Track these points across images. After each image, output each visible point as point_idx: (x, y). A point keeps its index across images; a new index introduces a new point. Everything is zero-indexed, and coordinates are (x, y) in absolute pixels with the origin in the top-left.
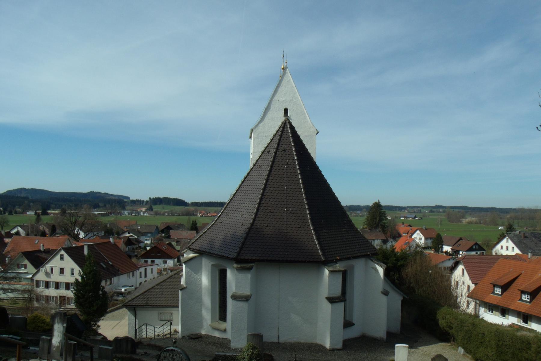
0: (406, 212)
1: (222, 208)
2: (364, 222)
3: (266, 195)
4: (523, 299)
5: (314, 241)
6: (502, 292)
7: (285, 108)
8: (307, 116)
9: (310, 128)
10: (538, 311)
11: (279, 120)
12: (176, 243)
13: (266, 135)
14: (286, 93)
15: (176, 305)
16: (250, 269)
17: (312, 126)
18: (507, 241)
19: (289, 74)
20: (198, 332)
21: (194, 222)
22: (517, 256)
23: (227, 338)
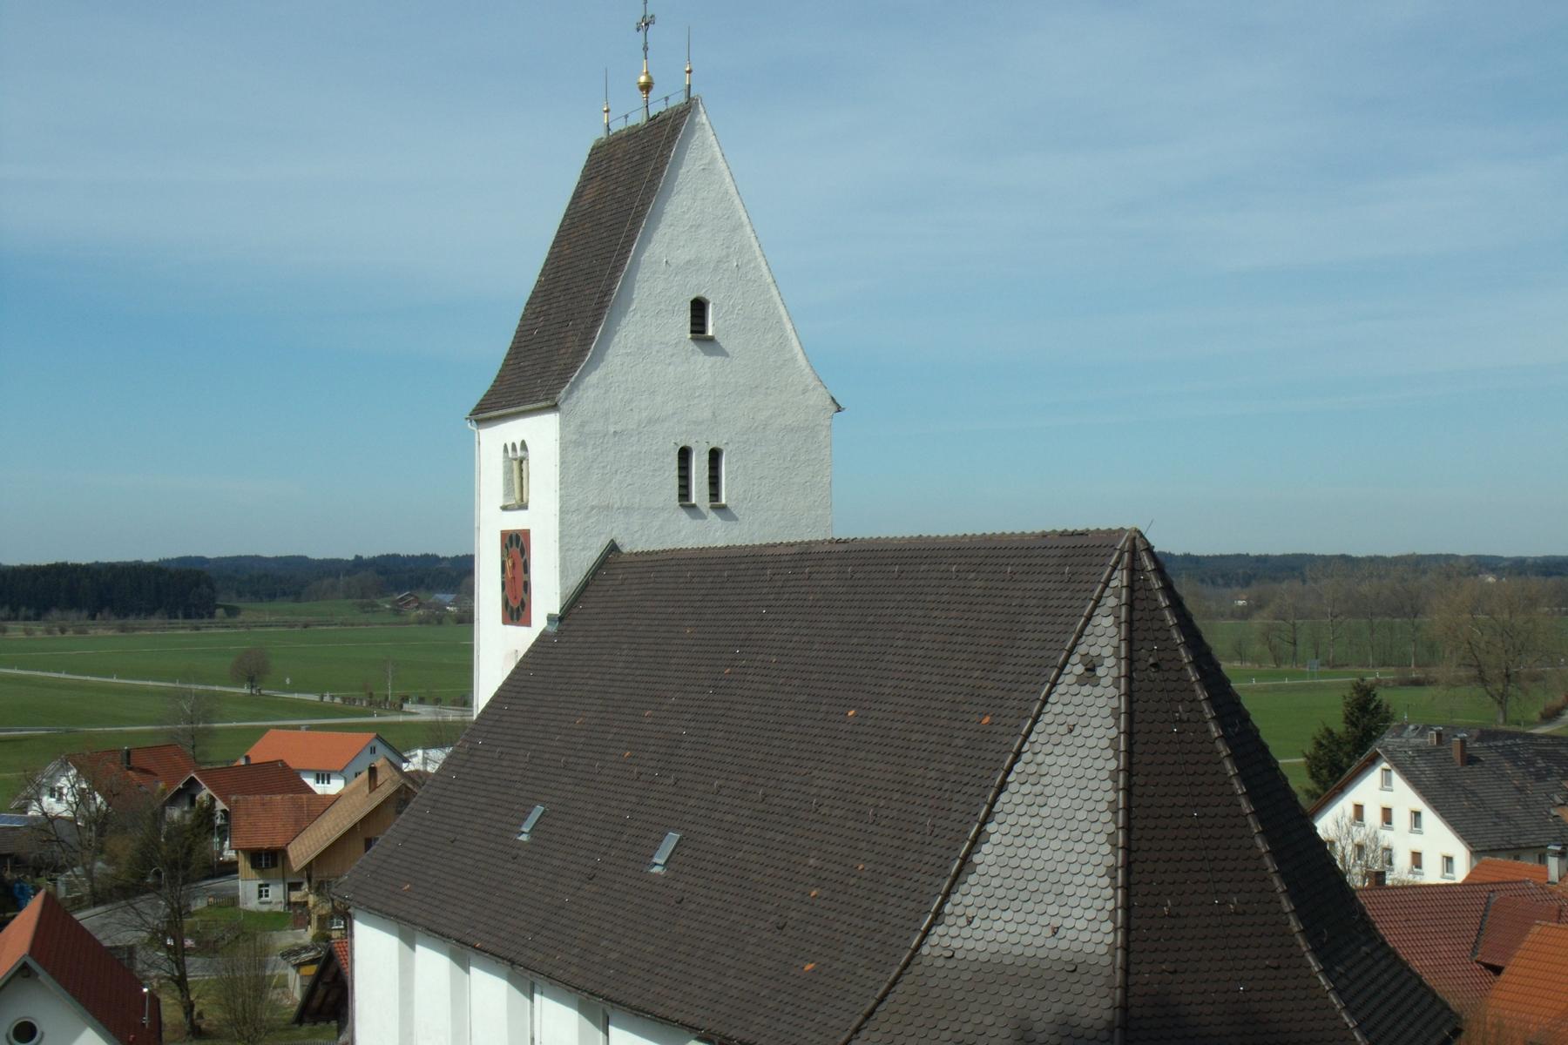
3: (1138, 849)
5: (1338, 1017)
7: (693, 296)
8: (792, 336)
9: (804, 392)
11: (672, 356)
13: (618, 428)
17: (810, 380)
18: (1387, 782)
19: (711, 132)
22: (1531, 885)
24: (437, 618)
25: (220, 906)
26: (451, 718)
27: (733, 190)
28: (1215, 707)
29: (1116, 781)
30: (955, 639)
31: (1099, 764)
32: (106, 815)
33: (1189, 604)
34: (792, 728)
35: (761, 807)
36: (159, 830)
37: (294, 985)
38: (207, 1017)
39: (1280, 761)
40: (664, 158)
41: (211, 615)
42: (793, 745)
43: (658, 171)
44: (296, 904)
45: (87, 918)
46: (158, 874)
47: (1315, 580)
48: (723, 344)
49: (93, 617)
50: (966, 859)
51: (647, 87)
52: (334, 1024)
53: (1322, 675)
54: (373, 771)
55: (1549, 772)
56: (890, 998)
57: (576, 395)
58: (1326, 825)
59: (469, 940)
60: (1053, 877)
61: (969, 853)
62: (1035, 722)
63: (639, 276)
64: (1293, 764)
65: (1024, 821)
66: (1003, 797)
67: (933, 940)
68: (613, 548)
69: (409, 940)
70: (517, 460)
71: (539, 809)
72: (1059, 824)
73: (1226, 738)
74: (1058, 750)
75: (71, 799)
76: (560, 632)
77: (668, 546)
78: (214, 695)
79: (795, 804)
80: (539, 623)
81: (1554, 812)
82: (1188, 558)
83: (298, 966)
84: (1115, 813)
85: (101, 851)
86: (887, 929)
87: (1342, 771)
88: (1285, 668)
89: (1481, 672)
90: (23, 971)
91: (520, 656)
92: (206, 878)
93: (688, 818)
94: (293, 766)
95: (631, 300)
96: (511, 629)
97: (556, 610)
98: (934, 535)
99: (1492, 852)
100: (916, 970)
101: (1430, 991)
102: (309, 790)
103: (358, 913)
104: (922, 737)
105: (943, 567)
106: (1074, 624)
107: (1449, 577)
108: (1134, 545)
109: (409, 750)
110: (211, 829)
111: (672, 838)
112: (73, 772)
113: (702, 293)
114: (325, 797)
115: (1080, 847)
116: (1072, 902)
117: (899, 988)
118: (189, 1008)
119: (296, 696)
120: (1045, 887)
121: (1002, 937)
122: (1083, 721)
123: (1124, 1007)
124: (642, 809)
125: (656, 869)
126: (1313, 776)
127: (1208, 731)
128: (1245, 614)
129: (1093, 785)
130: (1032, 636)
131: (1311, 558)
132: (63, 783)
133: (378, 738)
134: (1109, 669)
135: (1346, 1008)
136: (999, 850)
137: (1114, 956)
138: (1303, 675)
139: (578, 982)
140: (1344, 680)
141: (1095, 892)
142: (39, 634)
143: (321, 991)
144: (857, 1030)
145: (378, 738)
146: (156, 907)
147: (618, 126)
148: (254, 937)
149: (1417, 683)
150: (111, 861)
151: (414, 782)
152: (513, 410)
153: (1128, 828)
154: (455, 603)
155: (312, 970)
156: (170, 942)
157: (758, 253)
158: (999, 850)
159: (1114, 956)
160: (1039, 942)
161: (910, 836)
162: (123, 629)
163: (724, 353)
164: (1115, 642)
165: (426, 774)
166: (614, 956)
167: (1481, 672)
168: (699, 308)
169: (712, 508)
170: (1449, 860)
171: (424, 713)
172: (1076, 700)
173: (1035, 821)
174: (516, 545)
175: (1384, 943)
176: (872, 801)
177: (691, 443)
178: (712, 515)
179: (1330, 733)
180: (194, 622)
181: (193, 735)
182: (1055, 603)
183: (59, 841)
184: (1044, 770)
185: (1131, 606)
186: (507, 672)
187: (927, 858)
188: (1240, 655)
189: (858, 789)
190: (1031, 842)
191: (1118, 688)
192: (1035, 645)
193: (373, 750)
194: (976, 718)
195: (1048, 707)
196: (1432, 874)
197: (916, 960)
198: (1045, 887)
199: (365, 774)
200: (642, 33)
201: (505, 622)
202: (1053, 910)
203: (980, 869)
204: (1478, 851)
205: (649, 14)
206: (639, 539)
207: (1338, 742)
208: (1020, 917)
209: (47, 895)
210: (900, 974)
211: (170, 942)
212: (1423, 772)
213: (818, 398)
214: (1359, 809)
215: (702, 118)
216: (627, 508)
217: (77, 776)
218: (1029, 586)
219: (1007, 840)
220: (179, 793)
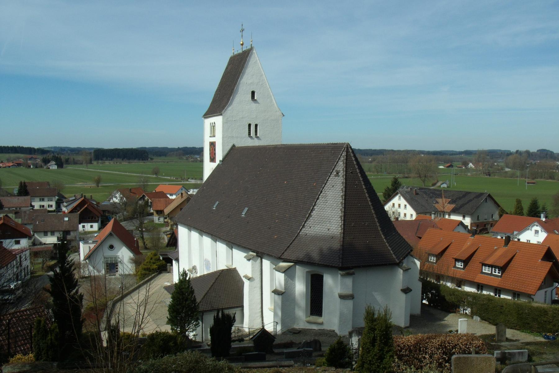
4: (457, 266)
5: (388, 248)
6: (465, 266)
7: (252, 90)
9: (276, 112)
10: (472, 276)
12: (14, 216)
13: (235, 119)
14: (253, 75)
15: (240, 305)
16: (353, 274)
17: (278, 109)
18: (400, 198)
20: (292, 327)
21: (23, 184)
24: (196, 161)
25: (150, 222)
26: (199, 183)
27: (261, 67)
28: (364, 182)
29: (342, 198)
30: (308, 166)
31: (339, 194)
32: (126, 202)
33: (359, 159)
34: (272, 185)
35: (265, 202)
36: (137, 206)
37: (166, 239)
38: (148, 245)
39: (378, 194)
40: (246, 60)
41: (147, 160)
42: (273, 189)
43: (245, 63)
44: (166, 222)
45: (123, 224)
46: (137, 215)
47: (386, 155)
48: (258, 101)
50: (310, 214)
51: (242, 45)
52: (174, 247)
53: (387, 176)
54: (182, 194)
55: (433, 197)
56: (293, 243)
57: (226, 112)
58: (387, 208)
59: (203, 230)
60: (328, 218)
61: (310, 213)
62: (325, 185)
63: (240, 86)
64: (380, 195)
65: (323, 206)
67: (302, 231)
68: (234, 146)
69: (190, 230)
70: (213, 126)
71: (218, 202)
72: (330, 207)
73: (366, 188)
74: (330, 191)
75: (119, 199)
76: (222, 164)
77: (246, 145)
78: (148, 177)
79: (273, 202)
80: (218, 162)
81: (433, 205)
82: (359, 150)
83: (167, 235)
84: (342, 204)
85: (125, 210)
86: (292, 229)
87: (390, 196)
88: (379, 174)
89: (420, 175)
90: (110, 234)
91: (214, 169)
92: (147, 216)
93: (250, 205)
94: (165, 192)
95: (238, 91)
96: (212, 163)
97: (221, 159)
98: (304, 143)
99: (421, 213)
100: (299, 238)
101: (407, 242)
102: (168, 198)
103: (179, 224)
104: (301, 188)
105: (306, 151)
106: (334, 163)
107: (414, 155)
109: (190, 189)
110: (148, 206)
111: (246, 209)
112: (119, 193)
113: (254, 90)
114: (172, 199)
115: (334, 212)
117: (295, 241)
118: (144, 243)
119: (165, 177)
120: (327, 220)
121: (317, 231)
122: (336, 185)
123: (343, 246)
124: (240, 202)
125: (243, 216)
126: (384, 197)
127: (362, 187)
128: (371, 162)
129: (337, 198)
130: (325, 166)
131: (385, 150)
132: (117, 195)
133: (183, 187)
134: (341, 173)
135: (389, 246)
136: (317, 212)
137: (341, 235)
138: (383, 175)
139: (226, 239)
140: (392, 177)
141: (337, 221)
143: (171, 240)
144: (286, 250)
145: (183, 187)
146: (137, 222)
147: (236, 53)
148: (157, 228)
149: (407, 177)
150: (127, 212)
151: (191, 196)
153: (345, 208)
154: (199, 158)
155: (169, 236)
156: (140, 229)
157: (266, 81)
158: (317, 212)
159: (341, 235)
160: (325, 232)
161: (298, 209)
162: (129, 163)
163: (258, 103)
164: (343, 167)
165: (193, 195)
166: (233, 234)
167: (420, 175)
168: (253, 93)
169: (256, 137)
170: (412, 215)
171: (193, 182)
172: (334, 180)
173: (325, 206)
174: (213, 145)
175: (398, 232)
176: (290, 201)
178: (256, 139)
179: (388, 188)
180: (144, 161)
181: (144, 185)
182: (330, 159)
183: (117, 207)
184: (327, 195)
185: (346, 159)
186: (211, 173)
187: (301, 214)
188: (369, 171)
189: (287, 199)
190: (324, 211)
191: (343, 177)
192: (326, 168)
193: (182, 189)
194: (312, 184)
195: (328, 181)
196: (408, 218)
197: (299, 235)
198: (327, 220)
199: (180, 195)
201: (210, 162)
202: (328, 225)
203: (313, 216)
204: (418, 213)
206: (239, 144)
207: (390, 190)
208: (321, 226)
209: (115, 219)
211: (140, 229)
212: (407, 197)
213: (279, 113)
214: (394, 204)
215: (254, 51)
217: (120, 194)
218: (324, 155)
219: (319, 210)
220: (141, 198)
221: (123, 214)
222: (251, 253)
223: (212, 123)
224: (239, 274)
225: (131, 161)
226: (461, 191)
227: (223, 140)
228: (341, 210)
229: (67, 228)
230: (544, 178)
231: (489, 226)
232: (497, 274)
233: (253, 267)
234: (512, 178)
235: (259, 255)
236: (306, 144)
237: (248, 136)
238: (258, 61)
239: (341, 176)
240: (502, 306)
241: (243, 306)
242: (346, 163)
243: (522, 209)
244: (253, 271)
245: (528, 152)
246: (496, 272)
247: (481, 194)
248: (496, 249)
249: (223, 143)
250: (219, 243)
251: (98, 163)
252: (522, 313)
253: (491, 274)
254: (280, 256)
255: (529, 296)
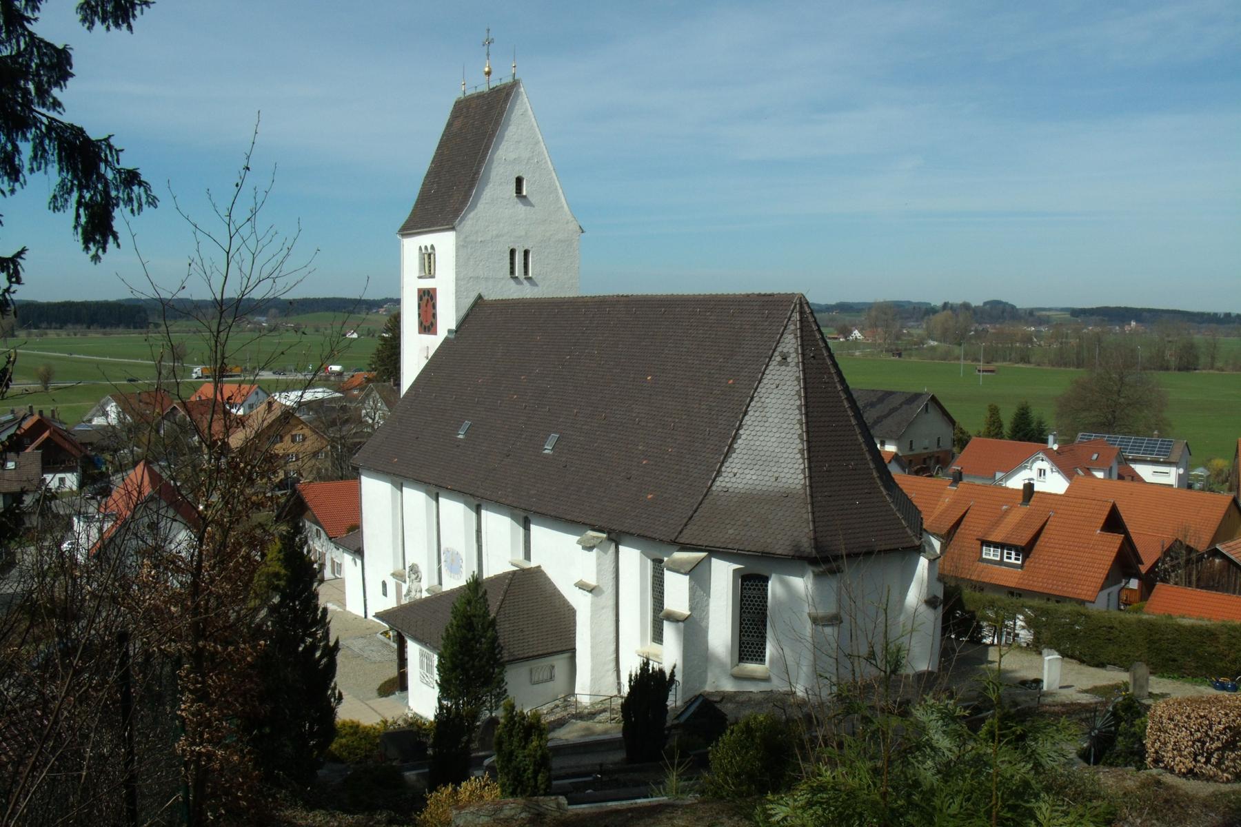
0: (382, 315)
1: (1165, 549)
2: (370, 365)
5: (895, 514)
9: (567, 223)
13: (483, 239)
17: (570, 217)
20: (702, 691)
23: (772, 691)
27: (535, 124)
49: (89, 328)
50: (731, 446)
51: (488, 73)
59: (441, 484)
62: (760, 383)
65: (758, 428)
66: (747, 418)
67: (718, 483)
68: (480, 297)
76: (456, 338)
77: (505, 297)
80: (442, 333)
84: (801, 425)
97: (453, 327)
100: (710, 497)
108: (801, 300)
116: (783, 465)
125: (546, 452)
127: (836, 387)
129: (789, 412)
133: (259, 387)
134: (794, 359)
142: (63, 336)
144: (686, 525)
152: (425, 230)
162: (105, 334)
168: (519, 181)
169: (525, 278)
173: (763, 429)
174: (427, 299)
177: (516, 247)
178: (525, 282)
184: (765, 405)
190: (761, 438)
191: (798, 367)
200: (486, 47)
201: (420, 333)
202: (774, 469)
203: (737, 451)
205: (490, 38)
206: (491, 295)
210: (703, 499)
213: (573, 226)
216: (486, 278)
221: (132, 452)
222: (591, 533)
223: (426, 248)
224: (549, 579)
225: (108, 330)
226: (873, 391)
227: (457, 284)
228: (800, 436)
229: (16, 488)
230: (1010, 360)
231: (933, 462)
232: (1013, 561)
233: (599, 565)
234: (945, 360)
235: (613, 535)
236: (686, 294)
237: (509, 276)
238: (530, 112)
239: (793, 364)
240: (1111, 628)
241: (575, 649)
242: (802, 337)
243: (1001, 426)
244: (599, 572)
245: (966, 306)
246: (1010, 558)
247: (917, 396)
248: (1006, 512)
249: (457, 291)
250: (488, 512)
251: (29, 335)
252: (1160, 639)
253: (1001, 562)
254: (676, 538)
255: (1082, 602)
